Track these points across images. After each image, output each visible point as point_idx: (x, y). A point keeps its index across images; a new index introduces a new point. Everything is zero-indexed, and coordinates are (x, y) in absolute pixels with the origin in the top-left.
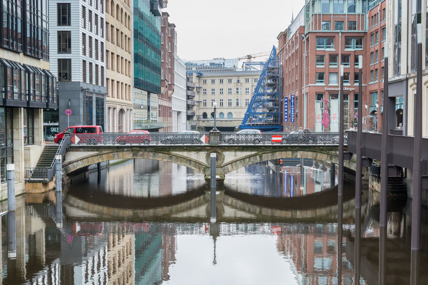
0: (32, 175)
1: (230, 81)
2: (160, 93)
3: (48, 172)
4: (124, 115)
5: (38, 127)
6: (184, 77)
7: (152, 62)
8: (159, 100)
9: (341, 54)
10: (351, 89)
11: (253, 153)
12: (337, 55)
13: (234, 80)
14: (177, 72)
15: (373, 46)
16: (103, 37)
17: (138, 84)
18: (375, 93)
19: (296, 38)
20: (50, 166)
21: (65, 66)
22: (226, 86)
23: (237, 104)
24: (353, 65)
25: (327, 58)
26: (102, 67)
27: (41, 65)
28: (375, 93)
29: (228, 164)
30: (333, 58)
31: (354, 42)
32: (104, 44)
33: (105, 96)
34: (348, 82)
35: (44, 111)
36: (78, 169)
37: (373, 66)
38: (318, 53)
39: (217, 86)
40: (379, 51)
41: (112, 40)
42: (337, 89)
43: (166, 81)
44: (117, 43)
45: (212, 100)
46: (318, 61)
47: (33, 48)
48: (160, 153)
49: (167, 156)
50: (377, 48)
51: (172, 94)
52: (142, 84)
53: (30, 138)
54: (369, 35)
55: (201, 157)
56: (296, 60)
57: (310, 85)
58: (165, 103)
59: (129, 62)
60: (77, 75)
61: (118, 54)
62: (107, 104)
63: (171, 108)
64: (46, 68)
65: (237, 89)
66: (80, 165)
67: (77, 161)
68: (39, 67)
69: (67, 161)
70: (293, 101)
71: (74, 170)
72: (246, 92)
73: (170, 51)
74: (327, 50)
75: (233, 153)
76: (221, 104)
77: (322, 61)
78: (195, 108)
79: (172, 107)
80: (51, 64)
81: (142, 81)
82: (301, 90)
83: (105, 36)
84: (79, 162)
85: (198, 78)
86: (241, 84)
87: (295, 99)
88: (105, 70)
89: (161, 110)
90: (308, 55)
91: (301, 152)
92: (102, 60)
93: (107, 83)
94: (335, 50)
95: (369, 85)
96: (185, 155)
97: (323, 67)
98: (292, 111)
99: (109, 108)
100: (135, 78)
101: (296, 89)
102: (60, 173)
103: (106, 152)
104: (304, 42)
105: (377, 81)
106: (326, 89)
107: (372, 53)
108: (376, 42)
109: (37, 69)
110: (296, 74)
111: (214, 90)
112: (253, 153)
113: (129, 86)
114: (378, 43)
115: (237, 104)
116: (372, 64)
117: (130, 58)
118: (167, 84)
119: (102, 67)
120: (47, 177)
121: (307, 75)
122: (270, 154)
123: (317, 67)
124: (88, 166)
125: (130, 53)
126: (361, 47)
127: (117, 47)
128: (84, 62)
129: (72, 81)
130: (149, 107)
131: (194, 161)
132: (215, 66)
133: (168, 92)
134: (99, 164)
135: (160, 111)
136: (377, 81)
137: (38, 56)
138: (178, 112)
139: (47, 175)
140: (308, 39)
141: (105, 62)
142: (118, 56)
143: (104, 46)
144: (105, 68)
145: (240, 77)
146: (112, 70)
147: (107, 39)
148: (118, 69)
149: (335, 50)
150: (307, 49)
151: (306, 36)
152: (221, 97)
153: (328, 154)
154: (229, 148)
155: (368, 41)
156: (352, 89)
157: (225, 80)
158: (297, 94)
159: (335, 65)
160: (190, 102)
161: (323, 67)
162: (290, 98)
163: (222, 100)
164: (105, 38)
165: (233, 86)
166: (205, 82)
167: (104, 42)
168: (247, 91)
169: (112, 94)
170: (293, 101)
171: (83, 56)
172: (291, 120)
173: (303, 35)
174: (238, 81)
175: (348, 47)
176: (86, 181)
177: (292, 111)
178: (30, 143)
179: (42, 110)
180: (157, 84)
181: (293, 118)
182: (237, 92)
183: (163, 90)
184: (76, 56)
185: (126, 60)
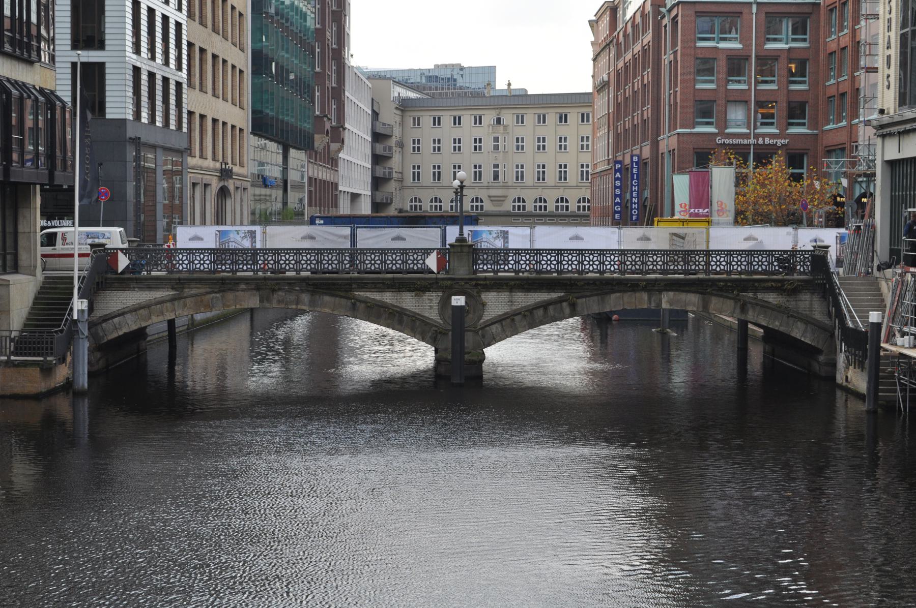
0: (16, 348)
1: (478, 120)
2: (313, 148)
3: (55, 341)
4: (229, 203)
5: (27, 230)
6: (366, 109)
7: (298, 75)
8: (310, 165)
9: (756, 56)
10: (780, 142)
11: (554, 296)
12: (747, 58)
13: (489, 118)
14: (351, 97)
15: (833, 37)
16: (180, 9)
17: (261, 126)
18: (838, 152)
19: (644, 15)
20: (59, 326)
21: (91, 79)
22: (468, 131)
23: (496, 177)
24: (785, 82)
25: (721, 66)
26: (179, 85)
27: (32, 76)
28: (838, 152)
29: (493, 324)
30: (736, 64)
31: (787, 26)
32: (184, 27)
33: (185, 155)
34: (772, 124)
35: (41, 191)
36: (125, 334)
37: (835, 87)
38: (700, 54)
39: (447, 131)
40: (849, 49)
41: (201, 17)
42: (746, 142)
43: (325, 119)
44: (213, 25)
45: (455, 167)
46: (700, 72)
47: (18, 36)
48: (326, 294)
49: (343, 301)
50: (845, 41)
51: (339, 150)
52: (272, 126)
53: (9, 257)
54: (822, 11)
55: (427, 306)
56: (644, 69)
57: (679, 130)
58: (323, 174)
59: (241, 72)
60: (118, 104)
61: (216, 53)
62: (190, 175)
63: (337, 185)
64: (48, 86)
65: (496, 139)
66: (130, 324)
67: (123, 314)
68: (32, 83)
69: (99, 313)
70: (635, 171)
71: (115, 335)
72: (475, 147)
73: (334, 46)
74: (723, 45)
75: (504, 296)
76: (478, 175)
77: (710, 71)
78: (392, 187)
79: (340, 184)
80: (58, 76)
81: (272, 118)
82: (655, 145)
83: (184, 7)
84: (128, 316)
85: (399, 112)
86: (506, 127)
87: (641, 164)
88: (184, 91)
89: (312, 189)
90: (675, 57)
91: (671, 294)
92: (179, 68)
93: (190, 123)
94: (740, 46)
95: (823, 131)
96: (388, 301)
97: (773, 87)
98: (634, 194)
99: (194, 185)
100: (253, 112)
101: (643, 141)
102: (84, 347)
103: (193, 291)
104: (665, 26)
105: (844, 123)
106: (719, 140)
107: (831, 54)
108: (841, 28)
109: (28, 88)
110: (644, 105)
111: (544, 139)
112: (554, 296)
113: (241, 130)
114: (846, 31)
115: (496, 177)
116: (832, 81)
117: (243, 60)
118: (328, 126)
119: (179, 85)
120: (52, 354)
121: (673, 107)
122: (595, 298)
123: (731, 87)
124: (146, 327)
125: (242, 50)
126: (805, 40)
127: (214, 34)
128: (137, 70)
129: (108, 116)
130: (285, 182)
131: (409, 316)
132: (439, 85)
133: (329, 147)
134: (171, 323)
135: (310, 192)
136: (844, 123)
137: (30, 56)
138: (352, 194)
139: (52, 349)
140: (674, 21)
141: (185, 71)
142: (215, 57)
143: (184, 32)
144: (185, 86)
145: (503, 111)
146: (201, 90)
147: (190, 15)
148: (214, 89)
149: (740, 46)
150: (674, 44)
151: (670, 11)
152: (478, 159)
153: (736, 299)
154: (498, 285)
155: (822, 24)
156: (783, 141)
157: (467, 119)
158: (647, 152)
159: (739, 82)
160: (380, 172)
161: (773, 87)
162: (627, 161)
163: (522, 167)
164: (185, 11)
165: (484, 132)
166: (417, 122)
167: (184, 23)
168: (478, 144)
169: (201, 150)
170: (635, 171)
171: (135, 56)
172: (632, 215)
173: (663, 10)
174: (499, 121)
175: (775, 40)
176: (139, 365)
177: (634, 194)
178: (8, 270)
179: (38, 187)
180: (307, 126)
181: (635, 212)
182: (496, 148)
183: (320, 141)
184: (121, 54)
185: (233, 67)
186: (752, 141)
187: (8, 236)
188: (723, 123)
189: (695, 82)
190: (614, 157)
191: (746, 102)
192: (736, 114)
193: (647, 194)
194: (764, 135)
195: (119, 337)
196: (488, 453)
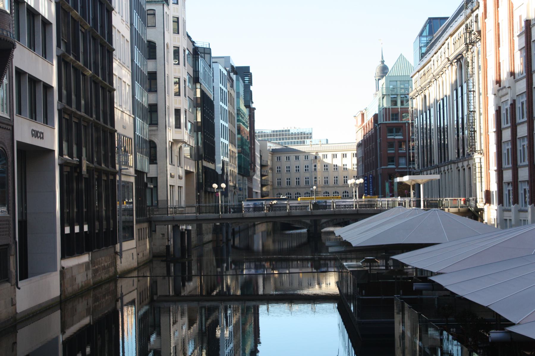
82: (376, 171)
106: (396, 170)
188: (398, 164)
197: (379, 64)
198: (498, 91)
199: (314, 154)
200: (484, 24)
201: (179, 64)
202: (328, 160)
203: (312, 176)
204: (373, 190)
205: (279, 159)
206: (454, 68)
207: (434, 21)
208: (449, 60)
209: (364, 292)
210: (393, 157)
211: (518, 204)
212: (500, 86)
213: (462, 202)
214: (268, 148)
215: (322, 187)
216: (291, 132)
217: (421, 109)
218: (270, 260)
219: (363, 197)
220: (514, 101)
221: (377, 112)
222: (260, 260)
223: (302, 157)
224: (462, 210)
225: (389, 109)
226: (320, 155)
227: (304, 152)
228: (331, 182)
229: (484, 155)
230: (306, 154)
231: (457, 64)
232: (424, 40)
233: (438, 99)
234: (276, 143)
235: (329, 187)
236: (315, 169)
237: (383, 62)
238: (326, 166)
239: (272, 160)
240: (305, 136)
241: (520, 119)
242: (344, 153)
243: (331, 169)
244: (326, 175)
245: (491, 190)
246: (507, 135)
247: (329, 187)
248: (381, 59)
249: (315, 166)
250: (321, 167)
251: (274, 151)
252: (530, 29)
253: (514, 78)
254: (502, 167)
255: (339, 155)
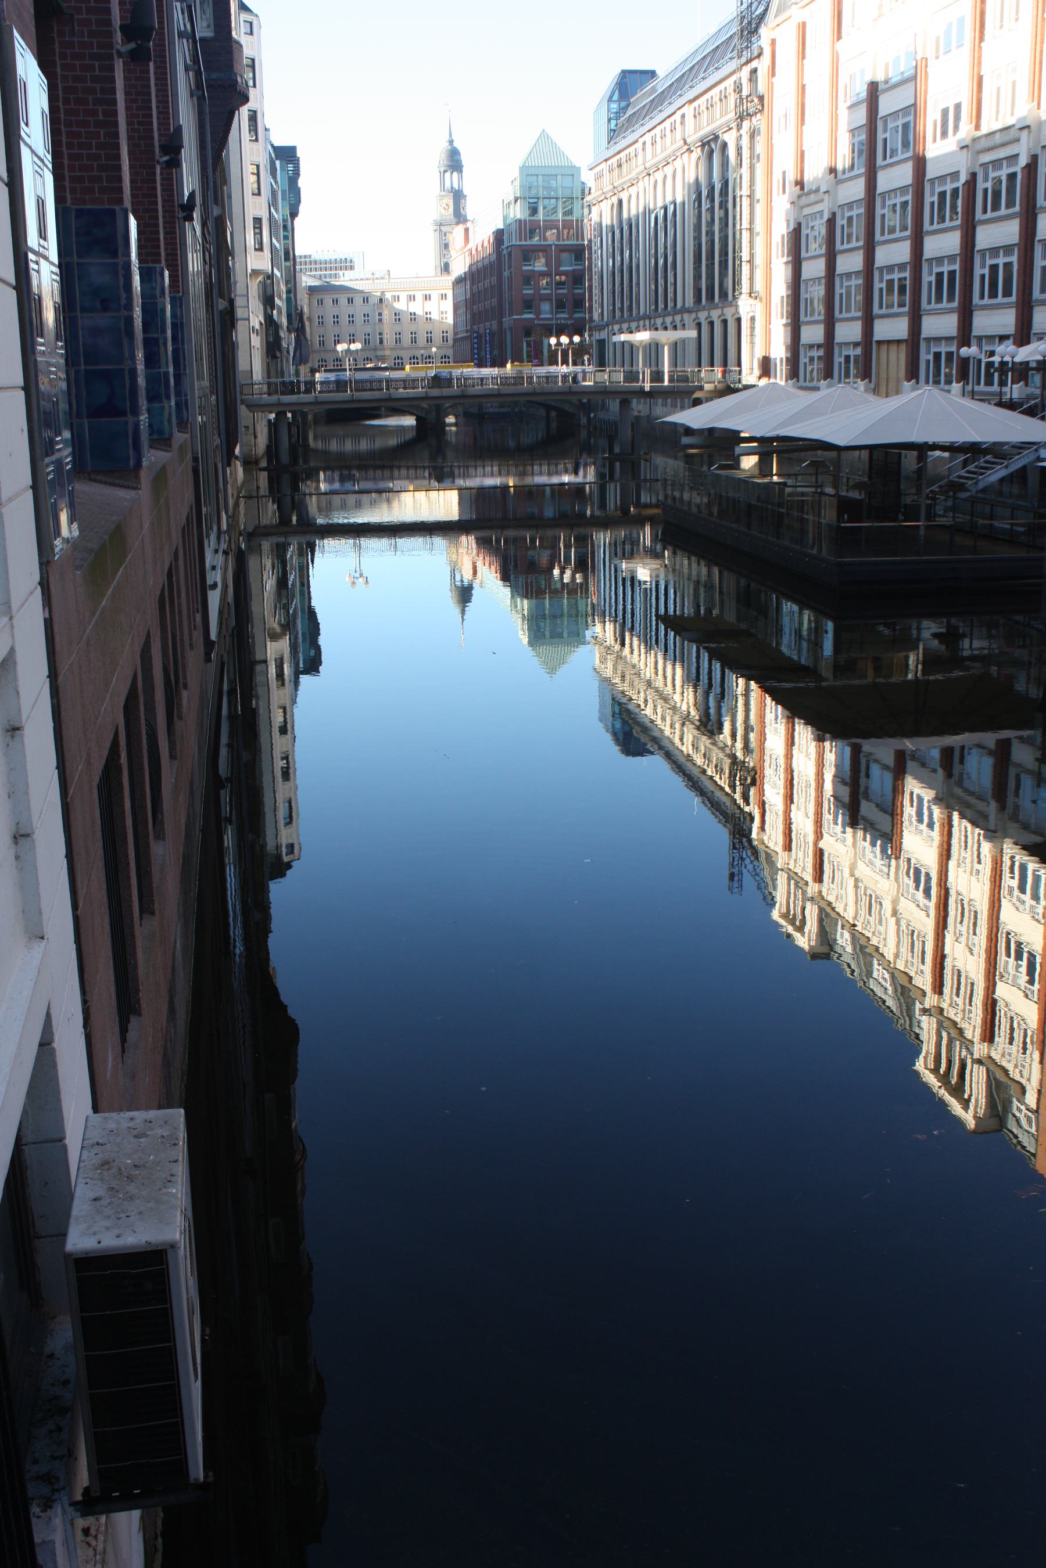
82: (500, 323)
97: (565, 291)
106: (536, 322)
115: (381, 342)
158: (495, 327)
161: (565, 291)
186: (554, 322)
187: (719, 680)
188: (538, 313)
189: (522, 289)
190: (472, 328)
191: (551, 300)
192: (545, 307)
193: (496, 352)
194: (561, 319)
195: (973, 729)
196: (782, 781)
197: (445, 145)
198: (799, 197)
199: (379, 294)
200: (771, 86)
201: (256, 140)
202: (401, 306)
203: (375, 332)
204: (491, 354)
205: (321, 302)
206: (694, 156)
207: (632, 75)
208: (685, 143)
209: (846, 516)
210: (531, 301)
211: (832, 378)
212: (802, 188)
213: (720, 375)
214: (304, 284)
215: (391, 349)
216: (313, 258)
217: (609, 223)
218: (359, 468)
219: (509, 366)
220: (834, 214)
221: (501, 227)
222: (349, 468)
223: (358, 300)
224: (720, 386)
225: (525, 221)
226: (388, 296)
227: (362, 292)
228: (406, 340)
229: (761, 300)
230: (366, 295)
231: (703, 151)
232: (614, 106)
233: (652, 207)
234: (314, 277)
235: (403, 349)
236: (380, 320)
237: (451, 142)
238: (397, 315)
239: (310, 305)
240: (347, 265)
241: (843, 243)
242: (428, 293)
243: (405, 319)
244: (398, 329)
245: (772, 356)
246: (814, 269)
247: (403, 349)
248: (447, 138)
249: (380, 314)
250: (390, 315)
251: (312, 290)
252: (877, 97)
253: (836, 177)
254: (833, 316)
255: (435, 295)
